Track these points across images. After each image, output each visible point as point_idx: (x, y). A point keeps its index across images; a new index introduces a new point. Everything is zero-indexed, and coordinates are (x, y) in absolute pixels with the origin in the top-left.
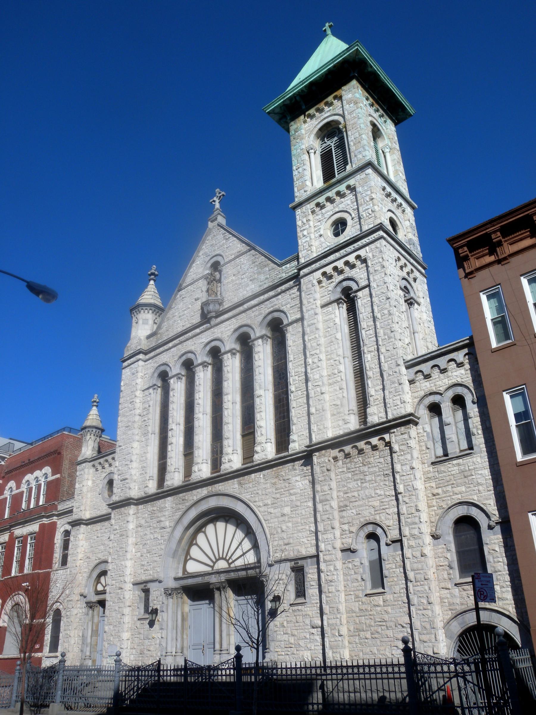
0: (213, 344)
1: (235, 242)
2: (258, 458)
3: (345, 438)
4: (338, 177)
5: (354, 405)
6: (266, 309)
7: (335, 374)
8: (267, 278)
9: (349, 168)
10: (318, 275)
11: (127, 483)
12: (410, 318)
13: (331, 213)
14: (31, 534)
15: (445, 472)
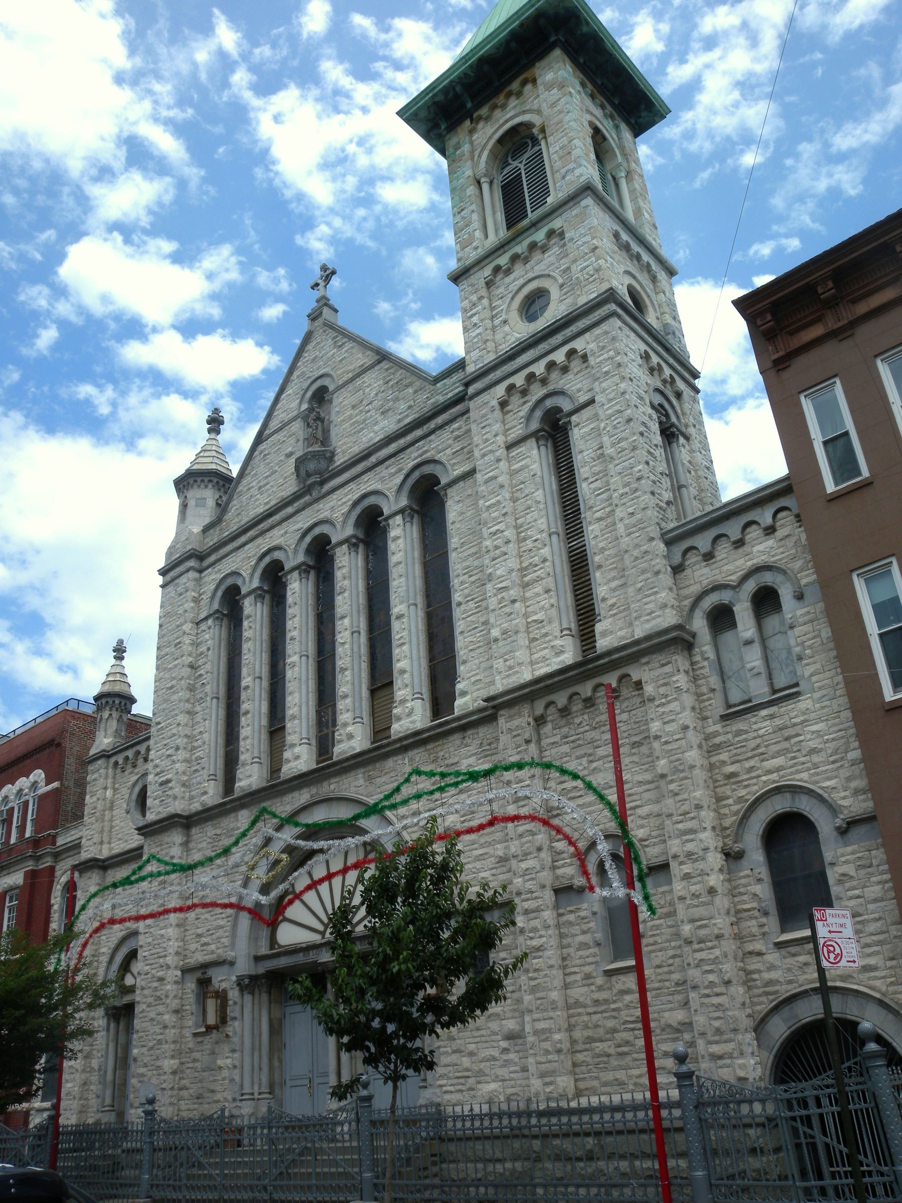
0: (317, 531)
1: (354, 351)
2: (398, 728)
3: (556, 679)
4: (532, 216)
5: (570, 620)
6: (409, 460)
7: (536, 565)
8: (410, 407)
9: (550, 200)
10: (500, 391)
11: (171, 788)
12: (671, 459)
13: (521, 281)
14: (11, 889)
15: (746, 732)
